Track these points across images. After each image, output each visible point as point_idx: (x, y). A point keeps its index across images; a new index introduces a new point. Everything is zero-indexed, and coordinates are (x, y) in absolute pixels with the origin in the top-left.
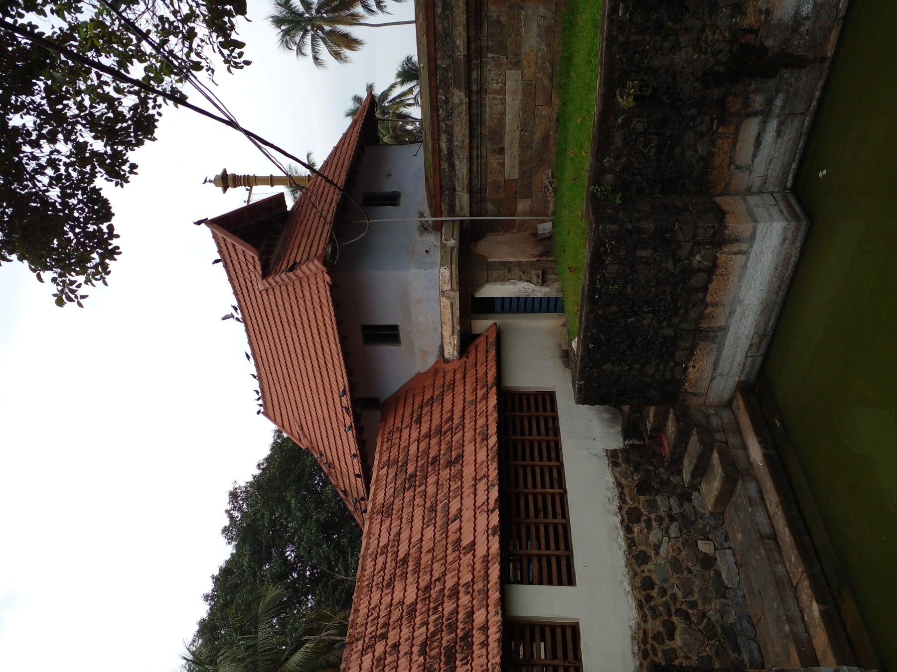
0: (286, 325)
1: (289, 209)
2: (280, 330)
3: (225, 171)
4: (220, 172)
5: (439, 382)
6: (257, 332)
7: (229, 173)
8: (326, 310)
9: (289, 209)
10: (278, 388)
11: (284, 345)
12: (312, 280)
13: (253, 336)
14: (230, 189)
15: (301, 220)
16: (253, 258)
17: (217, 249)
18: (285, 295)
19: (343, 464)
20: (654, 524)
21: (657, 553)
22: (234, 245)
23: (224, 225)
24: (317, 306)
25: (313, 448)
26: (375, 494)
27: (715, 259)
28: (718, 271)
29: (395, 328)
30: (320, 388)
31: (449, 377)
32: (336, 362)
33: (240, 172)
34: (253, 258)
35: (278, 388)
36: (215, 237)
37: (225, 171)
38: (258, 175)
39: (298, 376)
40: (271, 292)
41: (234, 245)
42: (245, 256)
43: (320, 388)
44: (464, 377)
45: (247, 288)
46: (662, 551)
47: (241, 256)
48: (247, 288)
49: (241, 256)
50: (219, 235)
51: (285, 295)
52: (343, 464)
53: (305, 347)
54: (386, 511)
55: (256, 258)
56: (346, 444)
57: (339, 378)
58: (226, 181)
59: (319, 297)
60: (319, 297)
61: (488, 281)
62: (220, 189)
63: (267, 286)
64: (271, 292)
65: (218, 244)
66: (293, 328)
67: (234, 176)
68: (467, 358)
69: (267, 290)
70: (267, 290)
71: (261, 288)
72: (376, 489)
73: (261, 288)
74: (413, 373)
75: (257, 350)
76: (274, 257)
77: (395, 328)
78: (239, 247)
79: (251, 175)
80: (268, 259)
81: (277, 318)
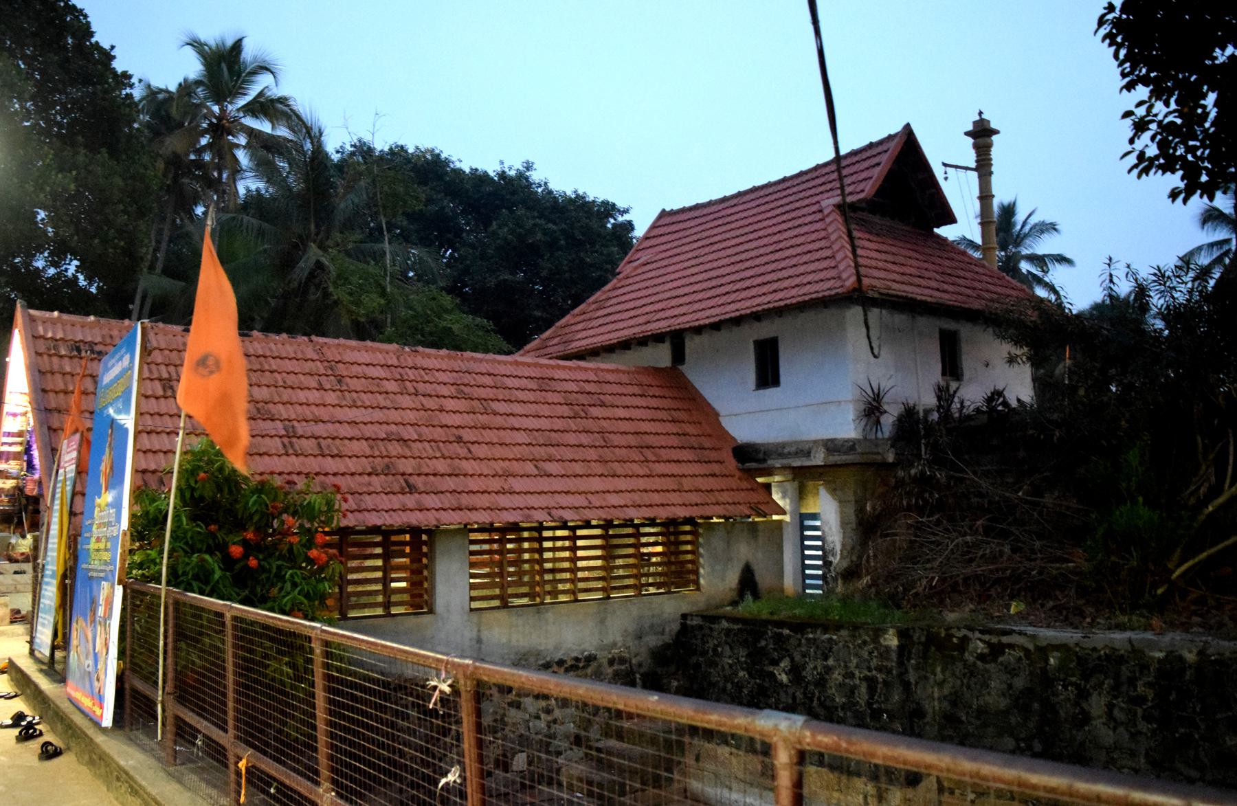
0: (776, 238)
1: (936, 230)
2: (770, 231)
3: (997, 132)
4: (993, 125)
5: (707, 443)
6: (767, 199)
7: (994, 138)
8: (794, 292)
9: (936, 230)
10: (696, 230)
11: (760, 218)
12: (833, 273)
13: (762, 193)
14: (970, 141)
15: (920, 249)
16: (862, 191)
17: (874, 140)
18: (814, 236)
19: (601, 321)
20: (543, 703)
21: (511, 704)
22: (878, 164)
23: (906, 150)
24: (797, 281)
25: (620, 280)
26: (564, 368)
27: (859, 775)
28: (844, 778)
29: (776, 382)
30: (696, 287)
31: (713, 455)
32: (728, 308)
33: (995, 153)
34: (862, 191)
35: (696, 230)
36: (890, 138)
37: (997, 132)
38: (994, 178)
39: (710, 257)
40: (819, 216)
41: (878, 164)
42: (865, 179)
43: (696, 287)
44: (713, 475)
45: (824, 183)
46: (513, 712)
47: (864, 175)
48: (824, 183)
49: (864, 175)
50: (892, 145)
51: (814, 236)
52: (601, 321)
53: (747, 264)
54: (544, 384)
55: (862, 196)
56: (625, 324)
57: (708, 313)
58: (982, 134)
59: (809, 283)
60: (809, 283)
61: (840, 502)
62: (970, 127)
63: (826, 212)
64: (819, 216)
65: (881, 142)
66: (771, 248)
67: (989, 146)
68: (740, 479)
69: (821, 211)
70: (821, 211)
71: (824, 204)
72: (570, 369)
73: (824, 204)
74: (717, 405)
75: (745, 199)
76: (865, 215)
77: (776, 382)
78: (876, 172)
79: (993, 169)
80: (863, 210)
81: (784, 226)
